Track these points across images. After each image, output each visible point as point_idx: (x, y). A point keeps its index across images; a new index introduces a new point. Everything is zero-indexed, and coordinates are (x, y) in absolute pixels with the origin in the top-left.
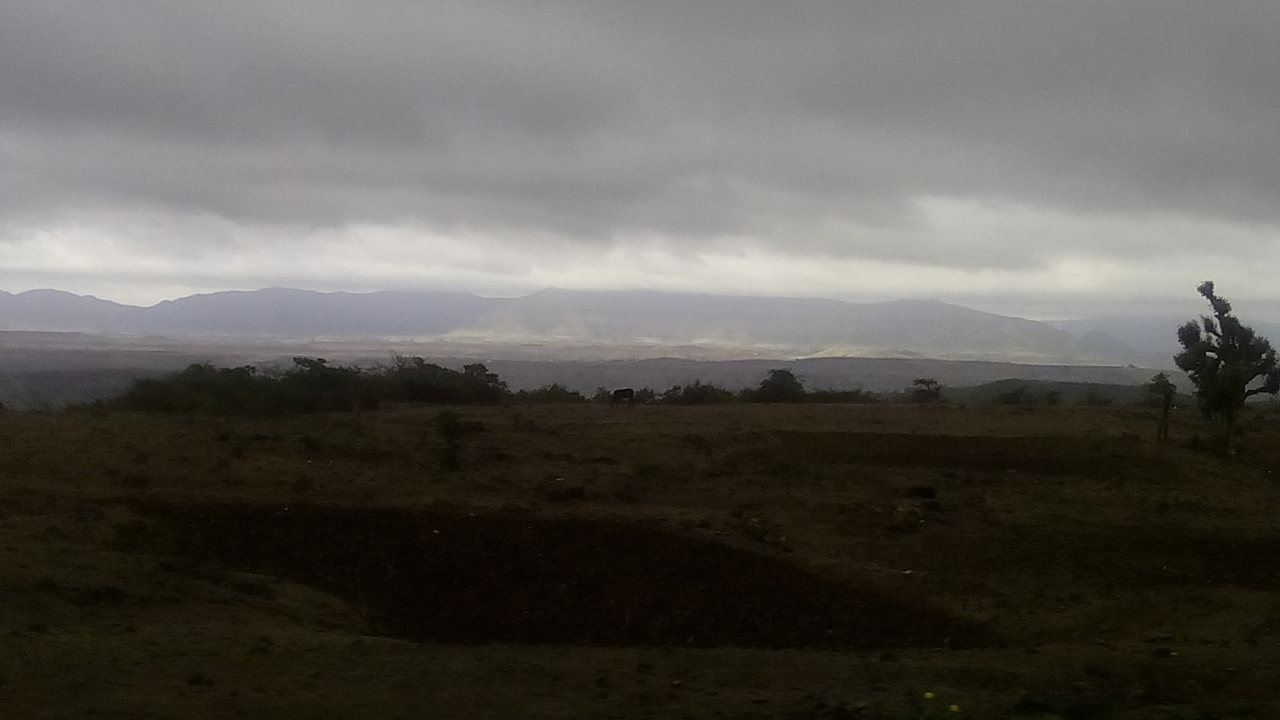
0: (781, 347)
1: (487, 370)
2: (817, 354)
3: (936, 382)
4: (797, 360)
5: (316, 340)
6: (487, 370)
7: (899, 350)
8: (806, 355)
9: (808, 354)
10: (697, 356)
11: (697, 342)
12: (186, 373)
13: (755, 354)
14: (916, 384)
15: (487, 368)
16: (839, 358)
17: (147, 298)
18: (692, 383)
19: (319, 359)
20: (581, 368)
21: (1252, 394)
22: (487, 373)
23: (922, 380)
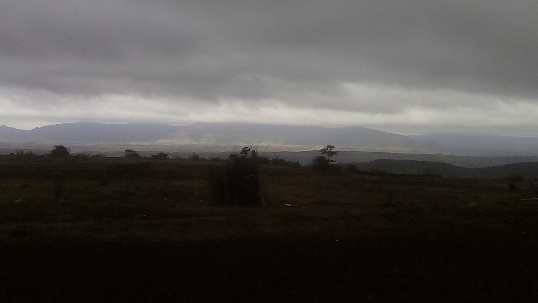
0: (297, 146)
8: (306, 149)
9: (309, 149)
11: (261, 144)
17: (29, 126)
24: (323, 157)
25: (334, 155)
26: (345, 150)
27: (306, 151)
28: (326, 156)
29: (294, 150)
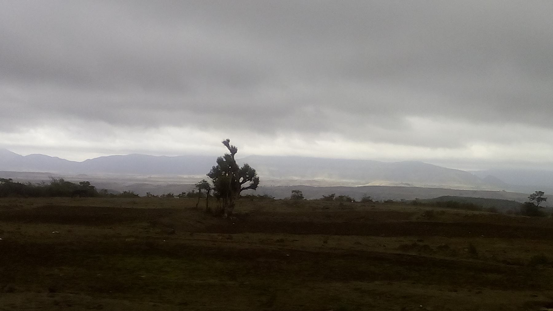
0: (353, 181)
1: (90, 185)
2: (368, 184)
3: (301, 192)
4: (358, 187)
5: (151, 177)
6: (90, 185)
7: (404, 183)
8: (363, 184)
9: (365, 184)
10: (316, 185)
11: (316, 179)
12: (285, 203)
13: (341, 184)
14: (292, 193)
15: (90, 183)
16: (377, 186)
17: (81, 158)
18: (191, 191)
19: (80, 183)
20: (175, 186)
21: (244, 189)
22: (89, 185)
23: (296, 191)
24: (533, 203)
25: (543, 202)
26: (403, 186)
27: (364, 186)
28: (535, 202)
29: (350, 185)
